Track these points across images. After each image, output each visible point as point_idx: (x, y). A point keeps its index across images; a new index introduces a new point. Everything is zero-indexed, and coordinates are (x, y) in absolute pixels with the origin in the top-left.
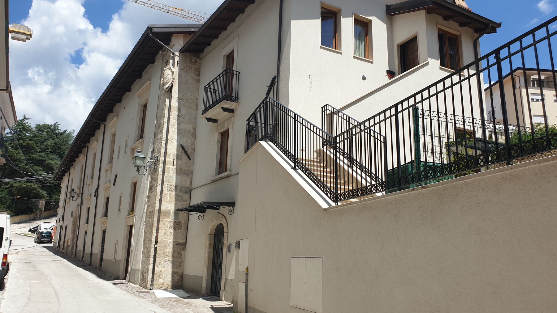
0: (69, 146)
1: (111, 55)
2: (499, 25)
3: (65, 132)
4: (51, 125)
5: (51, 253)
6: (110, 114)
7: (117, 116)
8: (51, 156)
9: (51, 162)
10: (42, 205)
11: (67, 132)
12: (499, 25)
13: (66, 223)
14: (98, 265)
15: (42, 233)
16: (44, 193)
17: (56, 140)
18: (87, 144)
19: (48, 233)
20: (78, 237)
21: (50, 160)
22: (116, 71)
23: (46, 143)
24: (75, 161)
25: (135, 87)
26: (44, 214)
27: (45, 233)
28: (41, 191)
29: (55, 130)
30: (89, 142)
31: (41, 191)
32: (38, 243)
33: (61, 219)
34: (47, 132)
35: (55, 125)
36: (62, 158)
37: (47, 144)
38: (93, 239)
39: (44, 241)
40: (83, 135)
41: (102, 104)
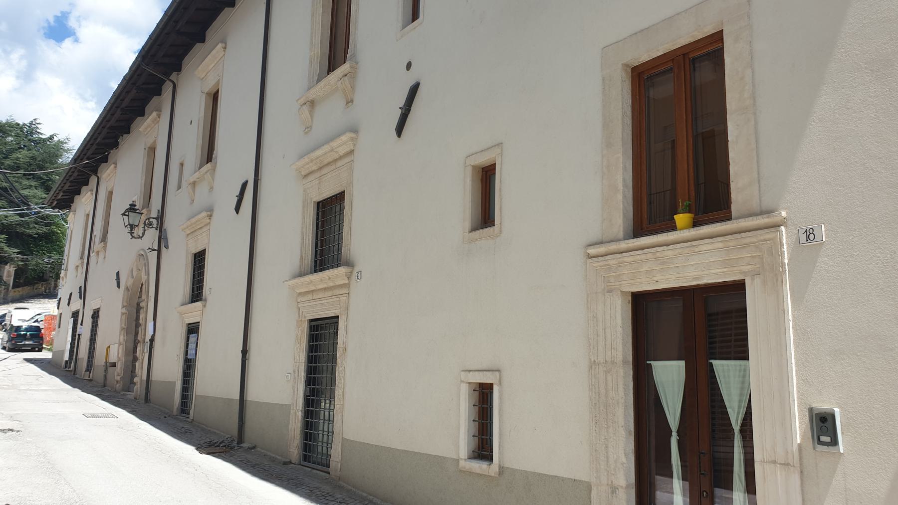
0: (62, 165)
1: (125, 28)
2: (718, 37)
3: (51, 137)
4: (24, 125)
5: (56, 381)
6: (198, 45)
7: (224, 41)
8: (26, 182)
9: (25, 192)
10: (9, 276)
11: (56, 139)
12: (718, 37)
13: (92, 304)
14: (294, 450)
15: (18, 328)
16: (12, 252)
17: (34, 152)
18: (173, 77)
19: (30, 329)
20: (152, 340)
21: (23, 189)
22: (132, 57)
23: (14, 156)
24: (116, 145)
25: (189, 62)
26: (13, 293)
27: (27, 330)
28: (6, 249)
29: (32, 133)
30: (178, 69)
31: (6, 249)
32: (10, 350)
33: (76, 295)
34: (17, 136)
35: (31, 123)
36: (47, 189)
37: (18, 159)
38: (245, 352)
39: (25, 345)
40: (119, 112)
41: (113, 115)
